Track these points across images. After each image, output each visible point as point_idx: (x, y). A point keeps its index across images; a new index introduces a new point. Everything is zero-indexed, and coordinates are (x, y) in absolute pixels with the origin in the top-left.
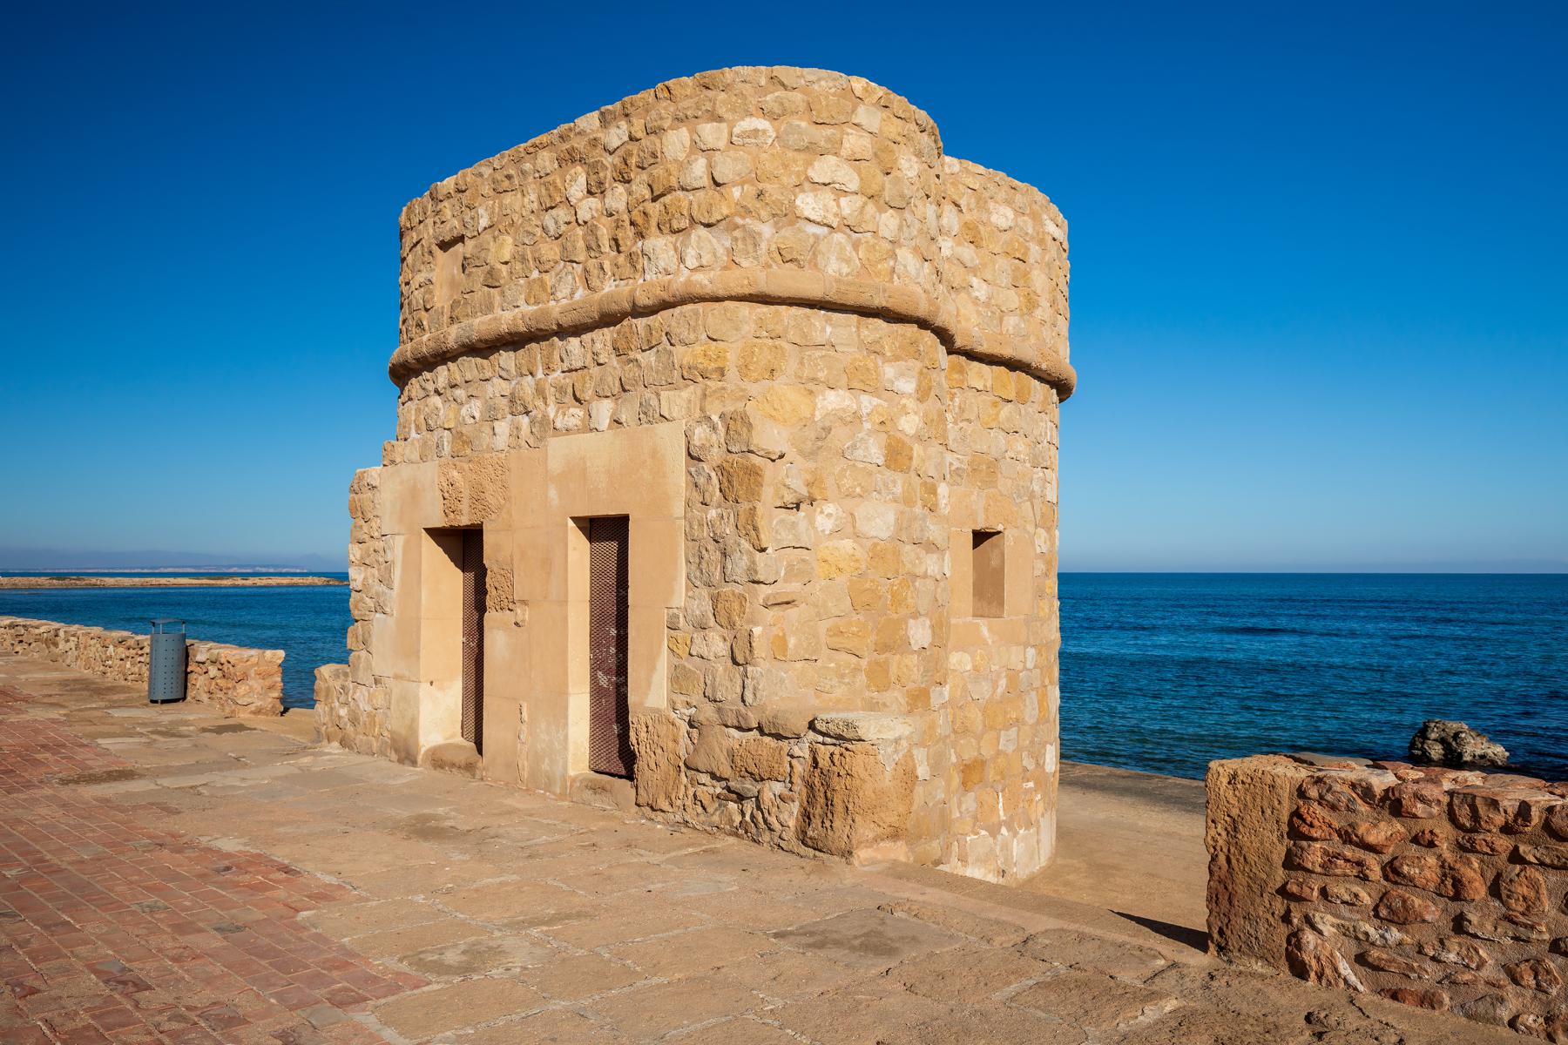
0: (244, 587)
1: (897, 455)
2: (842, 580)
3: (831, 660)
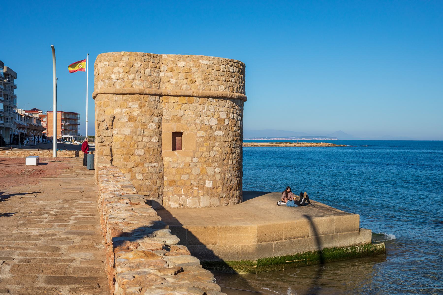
0: (290, 147)
1: (132, 119)
2: (119, 142)
3: (116, 156)
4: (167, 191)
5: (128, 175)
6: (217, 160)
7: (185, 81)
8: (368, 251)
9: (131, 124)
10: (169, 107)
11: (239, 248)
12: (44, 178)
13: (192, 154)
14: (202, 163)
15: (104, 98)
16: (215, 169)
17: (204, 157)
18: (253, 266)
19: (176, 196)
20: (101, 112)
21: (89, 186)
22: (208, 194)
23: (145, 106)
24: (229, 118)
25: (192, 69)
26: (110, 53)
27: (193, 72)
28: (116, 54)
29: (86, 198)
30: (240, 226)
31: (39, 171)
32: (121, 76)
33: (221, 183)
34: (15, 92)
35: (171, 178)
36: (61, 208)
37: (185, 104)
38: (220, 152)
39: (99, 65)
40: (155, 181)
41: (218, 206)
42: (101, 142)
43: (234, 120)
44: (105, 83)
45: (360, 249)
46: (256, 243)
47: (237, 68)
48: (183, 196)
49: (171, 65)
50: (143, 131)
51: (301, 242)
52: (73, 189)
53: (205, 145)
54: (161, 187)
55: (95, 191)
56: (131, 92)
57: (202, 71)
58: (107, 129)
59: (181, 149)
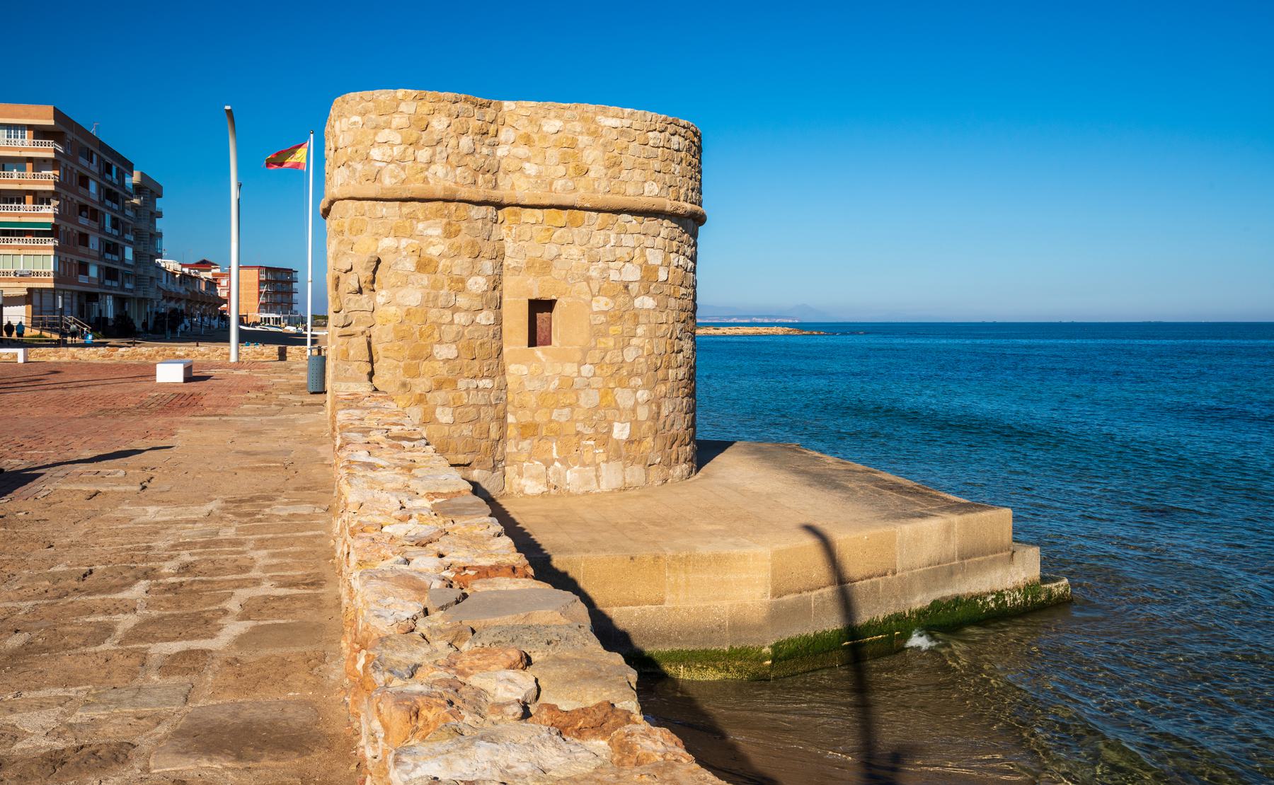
0: (715, 336)
1: (424, 265)
2: (390, 326)
3: (385, 362)
4: (515, 450)
5: (416, 413)
6: (640, 371)
7: (561, 170)
8: (1032, 602)
9: (425, 279)
10: (520, 236)
11: (725, 613)
12: (193, 418)
13: (578, 356)
14: (604, 378)
15: (351, 212)
16: (635, 392)
17: (610, 364)
18: (762, 661)
19: (537, 463)
20: (342, 248)
21: (308, 442)
22: (619, 457)
23: (460, 231)
24: (668, 266)
25: (580, 138)
26: (367, 94)
27: (581, 146)
28: (383, 95)
29: (296, 489)
30: (726, 552)
31: (186, 397)
32: (395, 154)
33: (650, 428)
34: (160, 224)
35: (526, 417)
36: (206, 545)
37: (562, 229)
38: (647, 349)
39: (337, 124)
40: (485, 426)
41: (643, 487)
42: (343, 327)
43: (680, 270)
44: (354, 170)
45: (1015, 599)
46: (768, 599)
47: (686, 139)
48: (557, 464)
49: (524, 127)
50: (454, 298)
51: (878, 588)
52: (264, 453)
53: (611, 332)
54: (501, 441)
55: (326, 462)
56: (423, 196)
57: (605, 146)
58: (360, 291)
59: (550, 344)
